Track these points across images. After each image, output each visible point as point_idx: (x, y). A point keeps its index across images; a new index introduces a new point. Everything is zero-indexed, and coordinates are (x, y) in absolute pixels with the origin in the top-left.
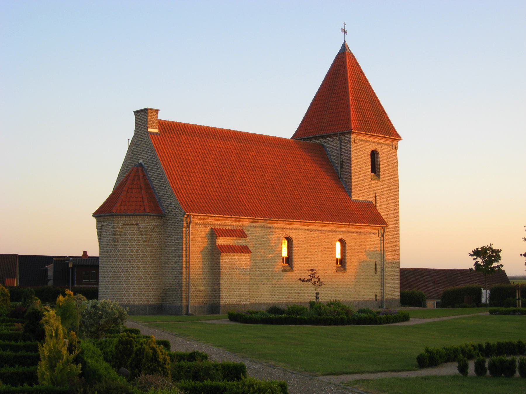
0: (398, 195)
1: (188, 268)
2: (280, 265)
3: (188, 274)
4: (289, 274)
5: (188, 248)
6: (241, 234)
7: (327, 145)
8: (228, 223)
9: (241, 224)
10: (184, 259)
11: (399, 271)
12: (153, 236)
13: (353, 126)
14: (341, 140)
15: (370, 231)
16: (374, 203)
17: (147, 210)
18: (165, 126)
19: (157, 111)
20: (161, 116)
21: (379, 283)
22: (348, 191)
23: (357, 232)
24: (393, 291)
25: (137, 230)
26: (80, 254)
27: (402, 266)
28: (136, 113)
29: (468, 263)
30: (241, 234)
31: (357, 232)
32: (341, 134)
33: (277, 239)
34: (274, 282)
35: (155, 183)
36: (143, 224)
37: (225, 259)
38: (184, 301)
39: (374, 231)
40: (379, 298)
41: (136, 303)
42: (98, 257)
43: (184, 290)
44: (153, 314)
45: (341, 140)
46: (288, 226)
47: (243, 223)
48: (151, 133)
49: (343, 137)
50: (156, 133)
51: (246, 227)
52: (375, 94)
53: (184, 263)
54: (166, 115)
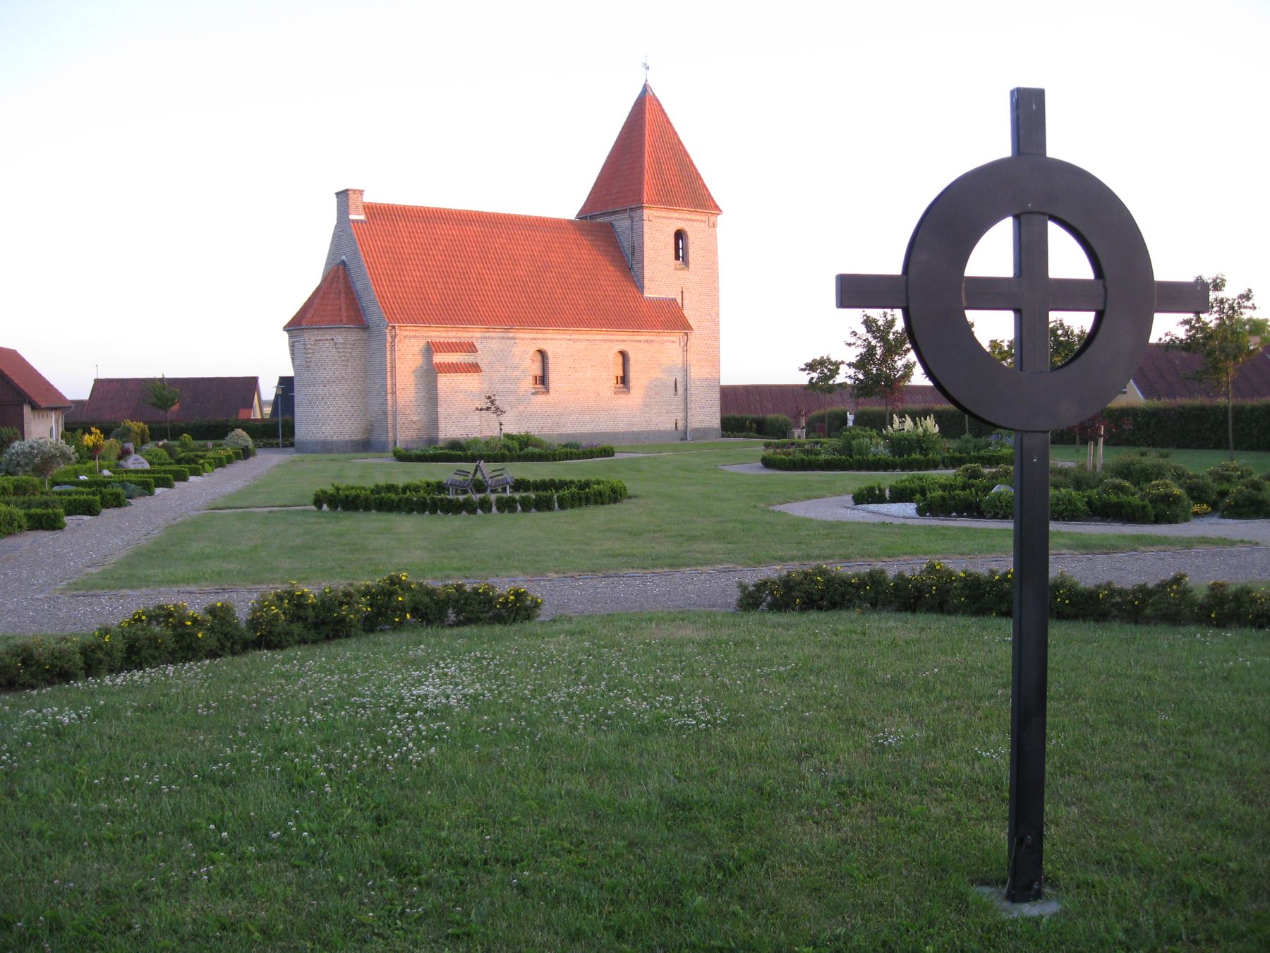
0: (717, 289)
1: (394, 393)
2: (527, 384)
3: (395, 401)
4: (541, 399)
5: (393, 367)
6: (471, 348)
7: (617, 224)
8: (451, 334)
9: (470, 335)
10: (389, 382)
11: (718, 390)
12: (354, 354)
13: (645, 198)
14: (632, 218)
15: (665, 338)
16: (679, 301)
17: (344, 320)
18: (371, 210)
19: (361, 192)
20: (368, 198)
21: (682, 407)
22: (641, 288)
23: (647, 341)
24: (708, 415)
25: (334, 346)
26: (1191, 279)
27: (723, 383)
28: (338, 194)
29: (803, 379)
30: (471, 348)
31: (647, 341)
32: (631, 210)
33: (508, 352)
34: (521, 408)
35: (359, 286)
36: (339, 339)
37: (444, 381)
38: (390, 434)
39: (673, 338)
40: (680, 427)
41: (335, 438)
42: (292, 378)
43: (390, 421)
44: (357, 451)
45: (632, 218)
46: (540, 336)
47: (474, 334)
48: (353, 221)
49: (633, 214)
50: (362, 221)
51: (477, 338)
52: (686, 152)
53: (389, 387)
54: (377, 195)
